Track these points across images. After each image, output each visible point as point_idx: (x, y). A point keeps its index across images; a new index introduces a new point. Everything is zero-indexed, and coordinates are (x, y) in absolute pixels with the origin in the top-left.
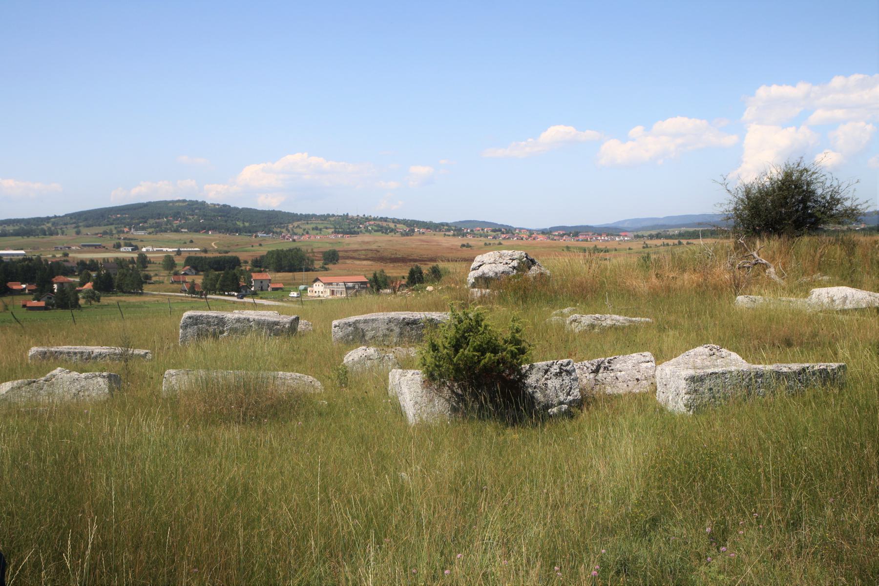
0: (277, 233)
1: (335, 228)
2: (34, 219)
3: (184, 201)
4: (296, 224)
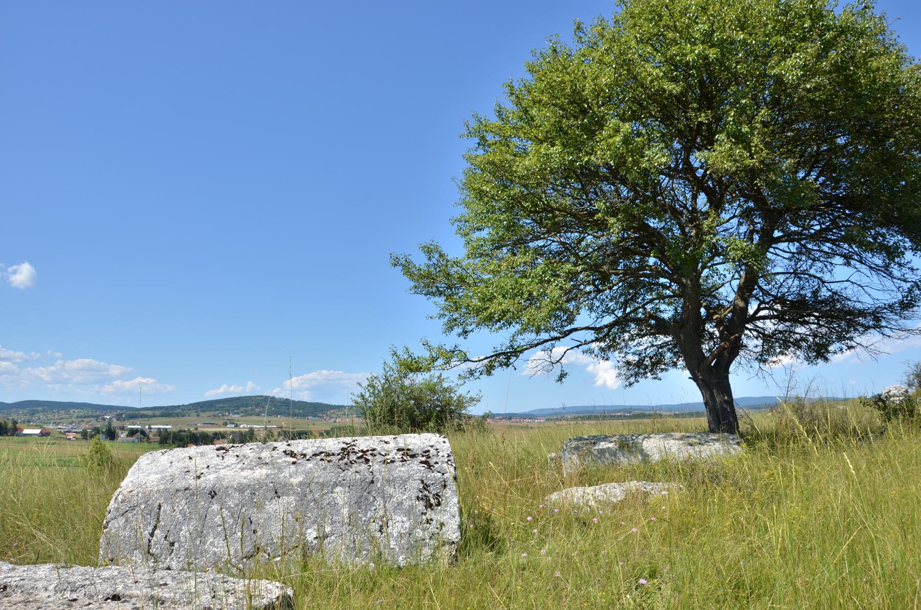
0: (320, 417)
1: (357, 414)
2: (170, 407)
3: (262, 396)
4: (332, 411)
